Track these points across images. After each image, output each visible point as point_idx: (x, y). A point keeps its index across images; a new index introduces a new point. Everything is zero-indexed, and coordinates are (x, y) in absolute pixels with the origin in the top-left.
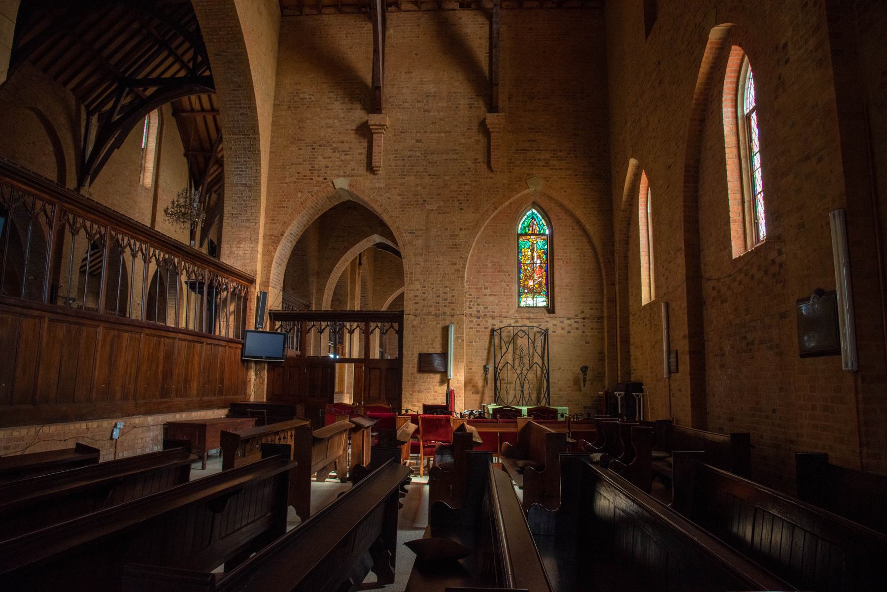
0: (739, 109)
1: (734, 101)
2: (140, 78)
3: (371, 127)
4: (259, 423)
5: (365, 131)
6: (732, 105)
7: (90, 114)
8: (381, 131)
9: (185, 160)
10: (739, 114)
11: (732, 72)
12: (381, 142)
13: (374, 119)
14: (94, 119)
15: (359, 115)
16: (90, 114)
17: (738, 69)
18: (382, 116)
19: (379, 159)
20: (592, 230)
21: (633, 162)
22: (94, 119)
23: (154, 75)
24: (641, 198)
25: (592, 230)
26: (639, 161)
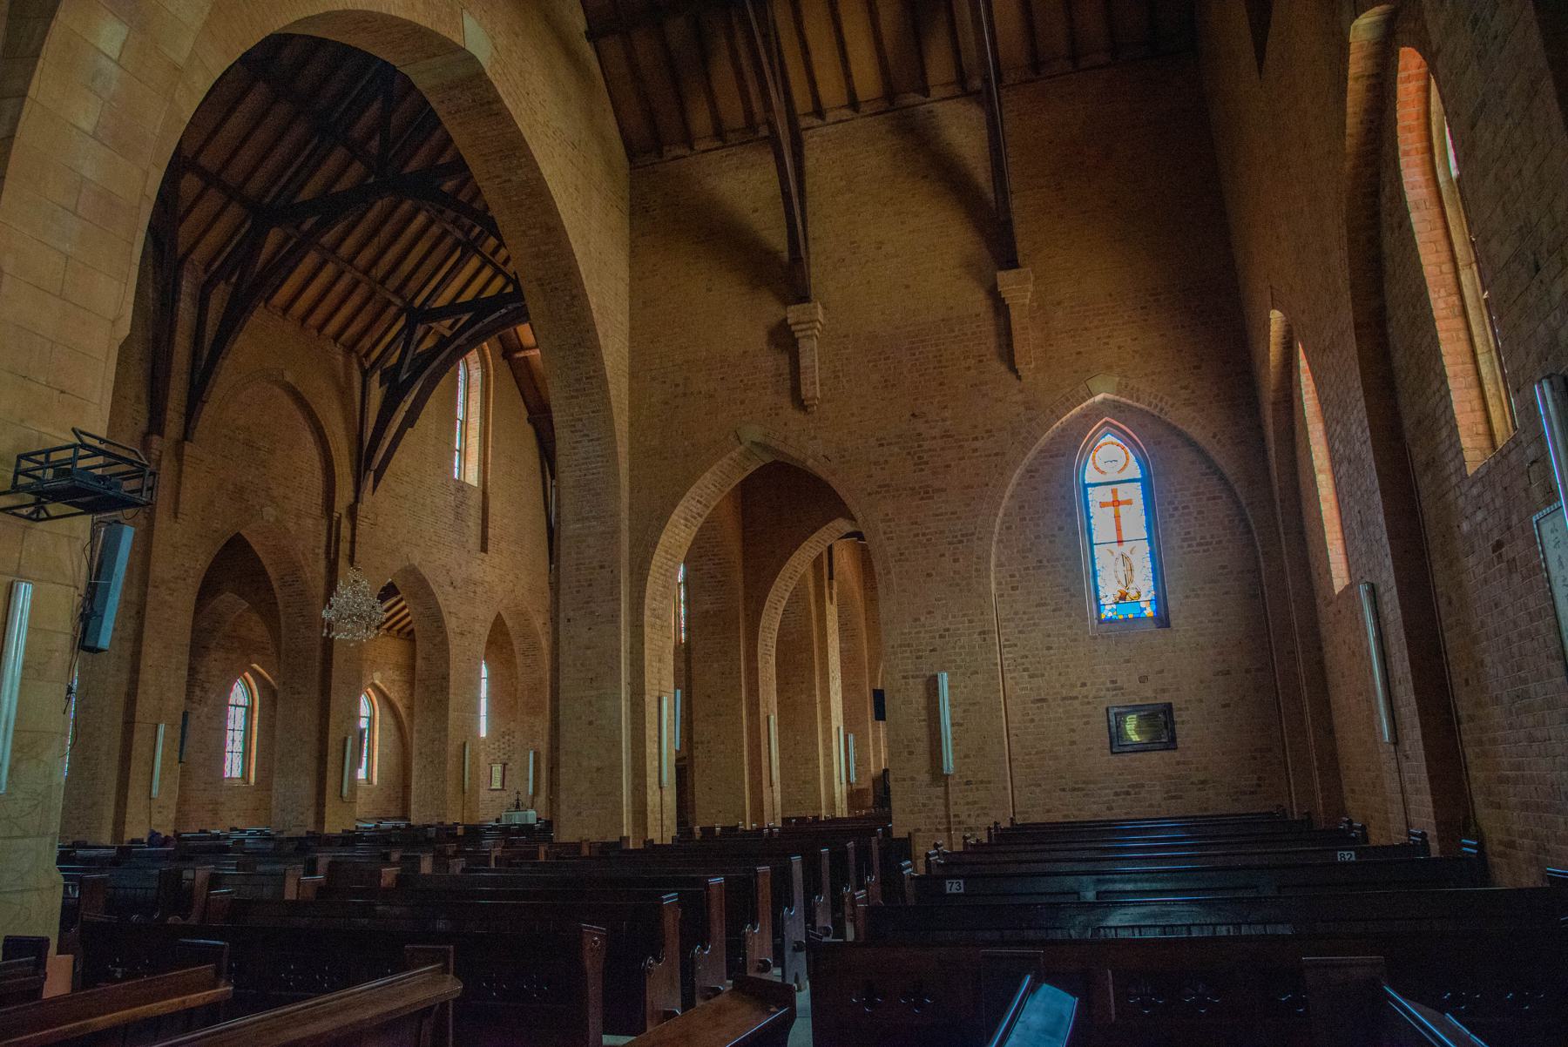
0: (1440, 171)
1: (1422, 116)
2: (490, 295)
3: (793, 328)
4: (704, 940)
5: (784, 339)
6: (1427, 180)
7: (366, 374)
8: (809, 332)
9: (530, 429)
10: (1441, 179)
11: (346, 527)
12: (811, 354)
13: (793, 313)
14: (375, 379)
15: (771, 310)
16: (366, 374)
17: (360, 495)
18: (811, 305)
19: (812, 388)
20: (1229, 469)
21: (1276, 316)
22: (375, 379)
23: (468, 295)
24: (1307, 393)
25: (1229, 469)
26: (1285, 315)
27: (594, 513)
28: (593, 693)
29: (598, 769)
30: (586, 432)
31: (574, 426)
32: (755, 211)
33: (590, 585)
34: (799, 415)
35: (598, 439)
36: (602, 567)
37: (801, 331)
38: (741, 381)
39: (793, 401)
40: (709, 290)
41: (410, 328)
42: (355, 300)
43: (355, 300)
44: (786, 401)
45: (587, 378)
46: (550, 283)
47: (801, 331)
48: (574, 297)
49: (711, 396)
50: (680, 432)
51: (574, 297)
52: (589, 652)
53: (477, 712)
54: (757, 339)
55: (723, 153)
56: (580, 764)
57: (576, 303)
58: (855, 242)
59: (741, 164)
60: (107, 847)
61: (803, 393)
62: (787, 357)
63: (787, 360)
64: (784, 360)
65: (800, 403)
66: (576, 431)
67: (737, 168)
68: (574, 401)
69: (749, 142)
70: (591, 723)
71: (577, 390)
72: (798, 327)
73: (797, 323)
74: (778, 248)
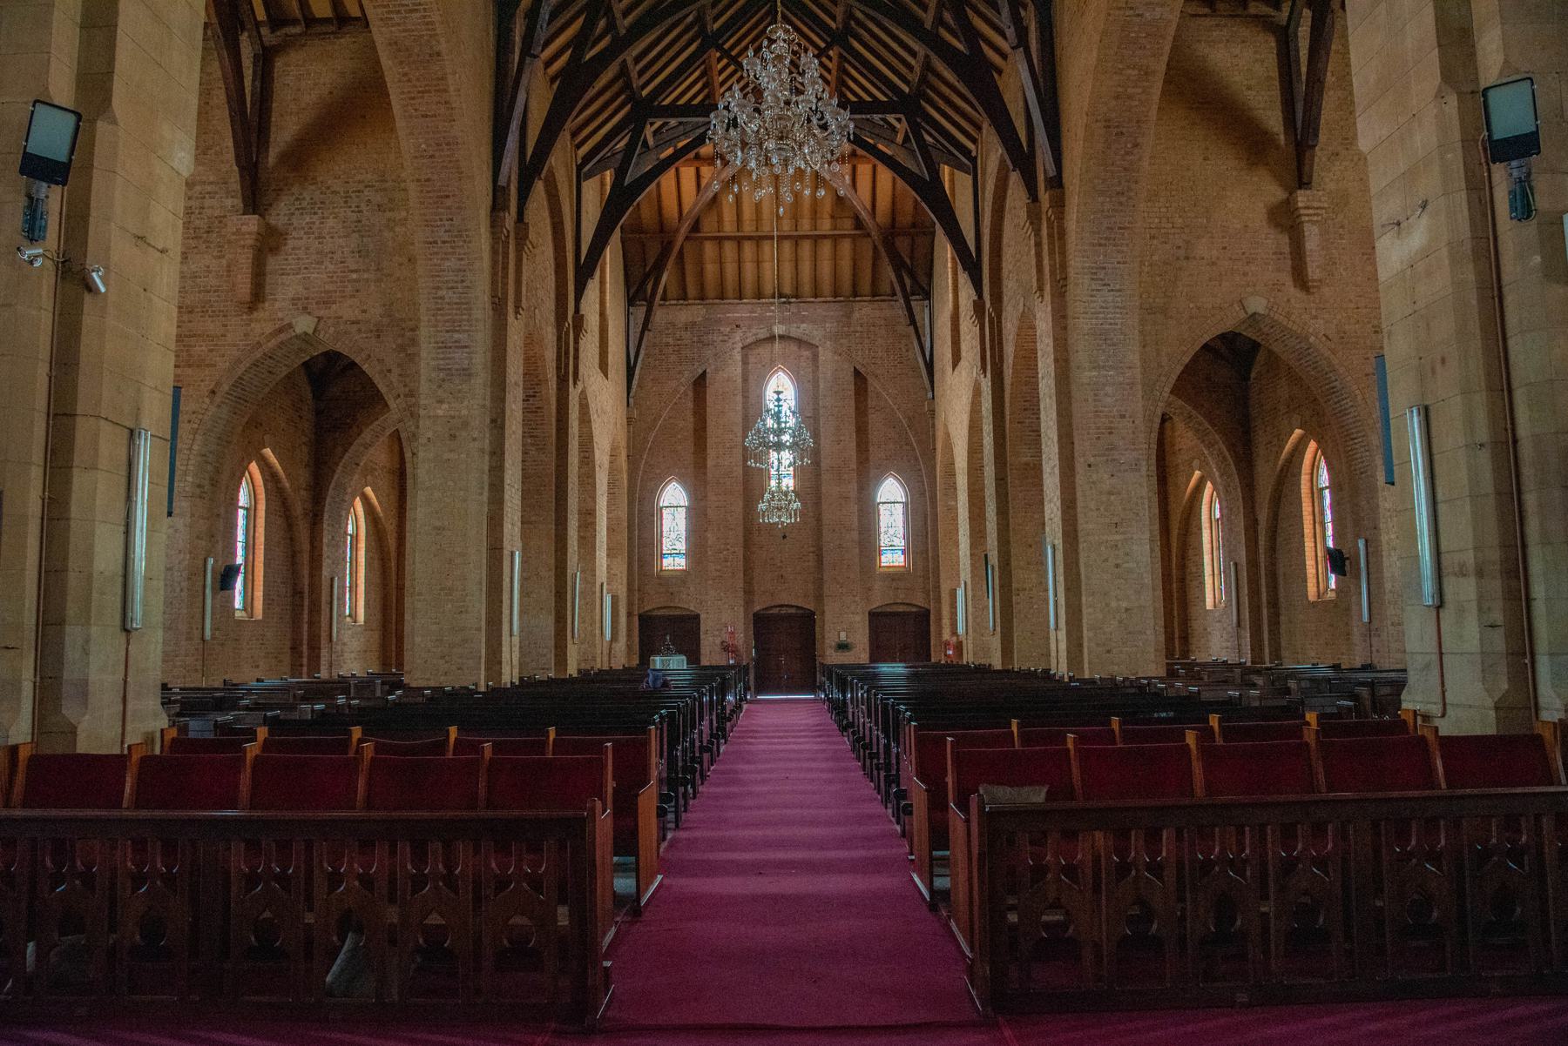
5: (1286, 219)
19: (1314, 271)
27: (1111, 363)
28: (1118, 537)
29: (1127, 610)
30: (1106, 282)
31: (1096, 273)
32: (1249, 88)
33: (1111, 433)
34: (1300, 294)
35: (1120, 290)
36: (1123, 416)
37: (1308, 215)
38: (1244, 253)
39: (1294, 280)
40: (1205, 159)
41: (635, 122)
42: (616, 88)
43: (616, 88)
44: (1287, 278)
45: (1120, 228)
46: (1117, 127)
47: (1308, 215)
48: (1136, 145)
49: (1214, 264)
50: (1184, 294)
51: (1136, 145)
52: (1112, 497)
53: (1046, 557)
54: (1257, 215)
55: (1208, 22)
56: (1107, 605)
57: (1136, 151)
58: (1347, 139)
59: (1232, 36)
60: (1188, 728)
61: (1310, 274)
62: (1287, 237)
63: (1287, 241)
64: (1284, 240)
65: (1300, 278)
66: (1097, 279)
67: (1228, 41)
68: (1102, 249)
69: (1237, 16)
70: (1117, 566)
71: (1106, 239)
72: (1306, 212)
73: (1308, 208)
74: (1275, 130)
